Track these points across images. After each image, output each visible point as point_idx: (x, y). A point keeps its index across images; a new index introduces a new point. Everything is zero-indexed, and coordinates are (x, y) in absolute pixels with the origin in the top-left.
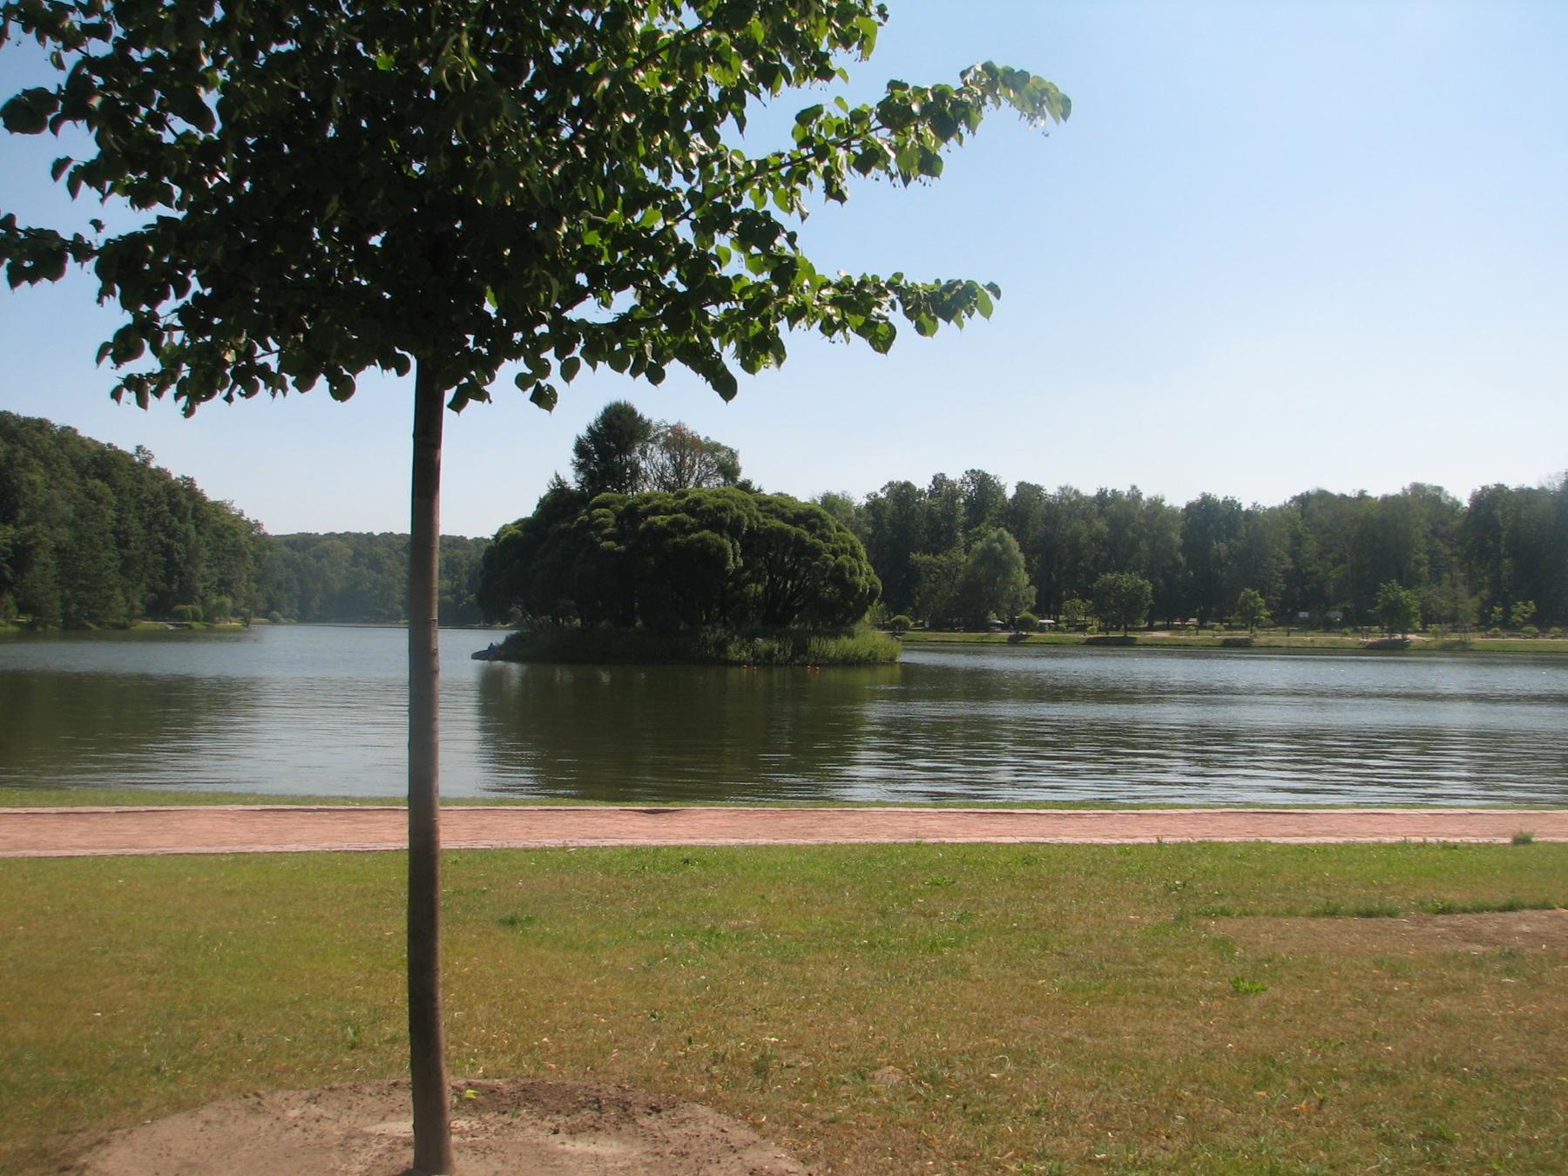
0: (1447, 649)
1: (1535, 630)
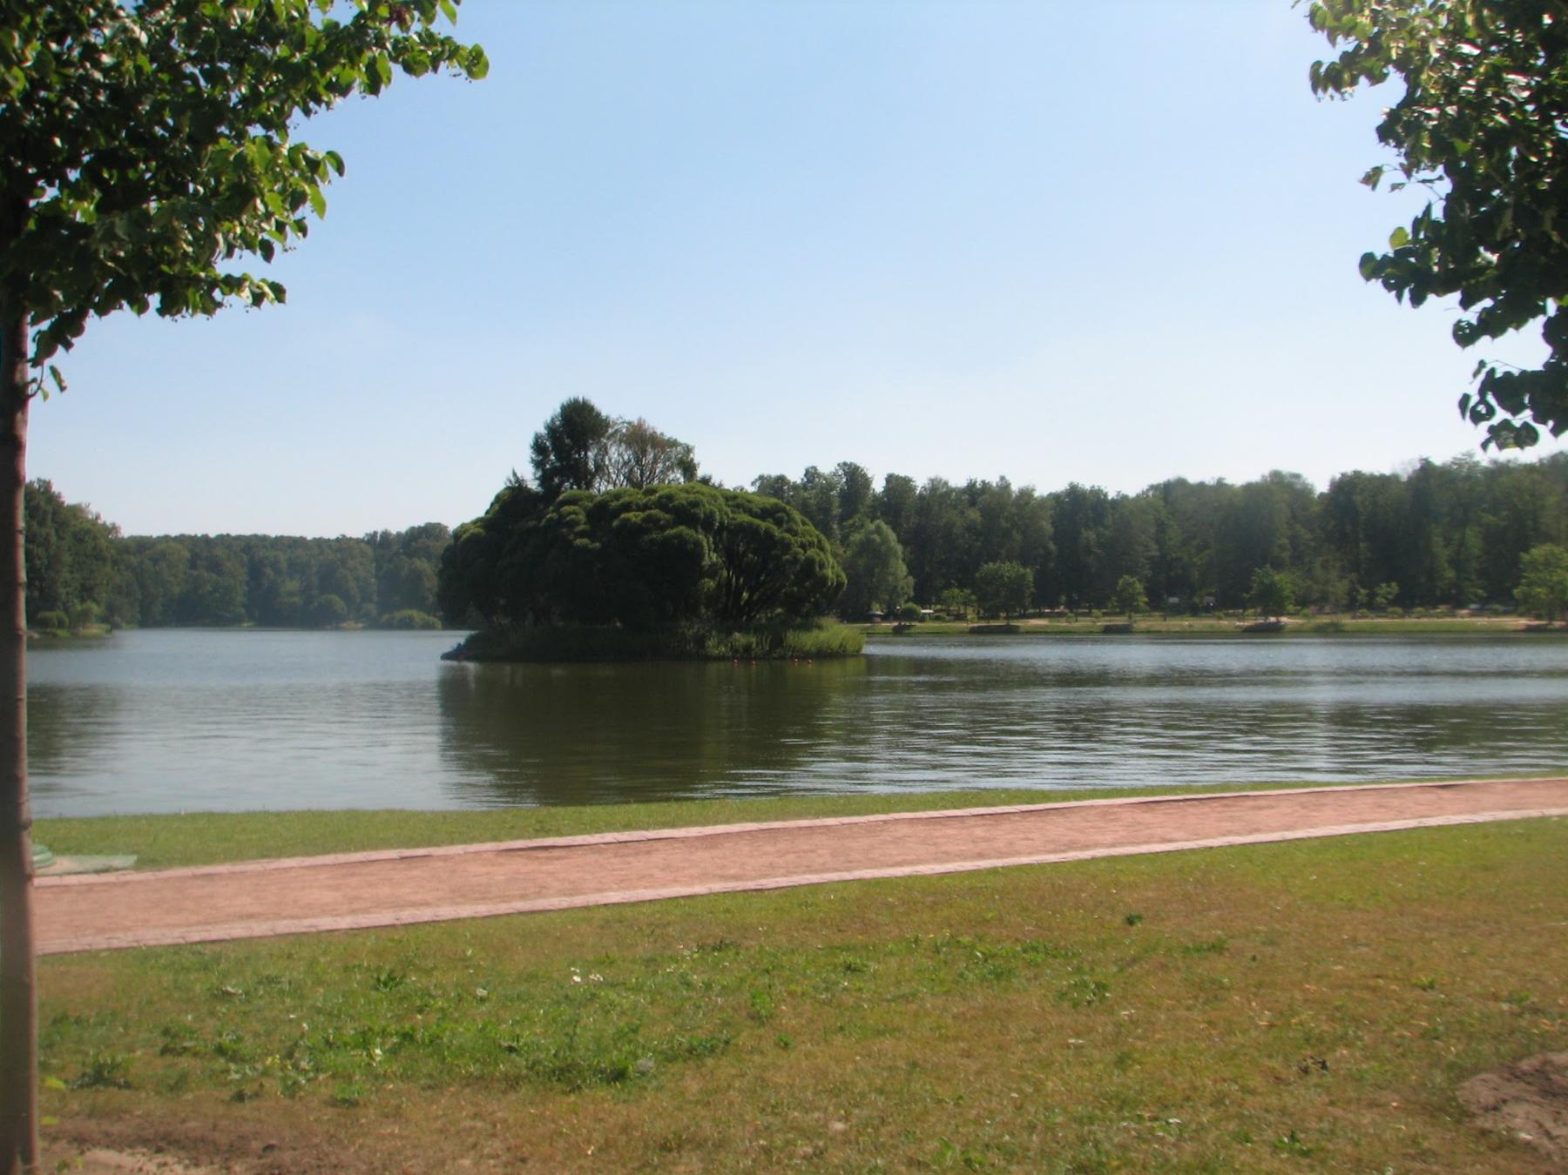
0: (1321, 631)
1: (1399, 610)
